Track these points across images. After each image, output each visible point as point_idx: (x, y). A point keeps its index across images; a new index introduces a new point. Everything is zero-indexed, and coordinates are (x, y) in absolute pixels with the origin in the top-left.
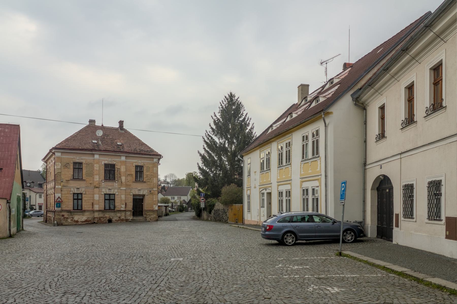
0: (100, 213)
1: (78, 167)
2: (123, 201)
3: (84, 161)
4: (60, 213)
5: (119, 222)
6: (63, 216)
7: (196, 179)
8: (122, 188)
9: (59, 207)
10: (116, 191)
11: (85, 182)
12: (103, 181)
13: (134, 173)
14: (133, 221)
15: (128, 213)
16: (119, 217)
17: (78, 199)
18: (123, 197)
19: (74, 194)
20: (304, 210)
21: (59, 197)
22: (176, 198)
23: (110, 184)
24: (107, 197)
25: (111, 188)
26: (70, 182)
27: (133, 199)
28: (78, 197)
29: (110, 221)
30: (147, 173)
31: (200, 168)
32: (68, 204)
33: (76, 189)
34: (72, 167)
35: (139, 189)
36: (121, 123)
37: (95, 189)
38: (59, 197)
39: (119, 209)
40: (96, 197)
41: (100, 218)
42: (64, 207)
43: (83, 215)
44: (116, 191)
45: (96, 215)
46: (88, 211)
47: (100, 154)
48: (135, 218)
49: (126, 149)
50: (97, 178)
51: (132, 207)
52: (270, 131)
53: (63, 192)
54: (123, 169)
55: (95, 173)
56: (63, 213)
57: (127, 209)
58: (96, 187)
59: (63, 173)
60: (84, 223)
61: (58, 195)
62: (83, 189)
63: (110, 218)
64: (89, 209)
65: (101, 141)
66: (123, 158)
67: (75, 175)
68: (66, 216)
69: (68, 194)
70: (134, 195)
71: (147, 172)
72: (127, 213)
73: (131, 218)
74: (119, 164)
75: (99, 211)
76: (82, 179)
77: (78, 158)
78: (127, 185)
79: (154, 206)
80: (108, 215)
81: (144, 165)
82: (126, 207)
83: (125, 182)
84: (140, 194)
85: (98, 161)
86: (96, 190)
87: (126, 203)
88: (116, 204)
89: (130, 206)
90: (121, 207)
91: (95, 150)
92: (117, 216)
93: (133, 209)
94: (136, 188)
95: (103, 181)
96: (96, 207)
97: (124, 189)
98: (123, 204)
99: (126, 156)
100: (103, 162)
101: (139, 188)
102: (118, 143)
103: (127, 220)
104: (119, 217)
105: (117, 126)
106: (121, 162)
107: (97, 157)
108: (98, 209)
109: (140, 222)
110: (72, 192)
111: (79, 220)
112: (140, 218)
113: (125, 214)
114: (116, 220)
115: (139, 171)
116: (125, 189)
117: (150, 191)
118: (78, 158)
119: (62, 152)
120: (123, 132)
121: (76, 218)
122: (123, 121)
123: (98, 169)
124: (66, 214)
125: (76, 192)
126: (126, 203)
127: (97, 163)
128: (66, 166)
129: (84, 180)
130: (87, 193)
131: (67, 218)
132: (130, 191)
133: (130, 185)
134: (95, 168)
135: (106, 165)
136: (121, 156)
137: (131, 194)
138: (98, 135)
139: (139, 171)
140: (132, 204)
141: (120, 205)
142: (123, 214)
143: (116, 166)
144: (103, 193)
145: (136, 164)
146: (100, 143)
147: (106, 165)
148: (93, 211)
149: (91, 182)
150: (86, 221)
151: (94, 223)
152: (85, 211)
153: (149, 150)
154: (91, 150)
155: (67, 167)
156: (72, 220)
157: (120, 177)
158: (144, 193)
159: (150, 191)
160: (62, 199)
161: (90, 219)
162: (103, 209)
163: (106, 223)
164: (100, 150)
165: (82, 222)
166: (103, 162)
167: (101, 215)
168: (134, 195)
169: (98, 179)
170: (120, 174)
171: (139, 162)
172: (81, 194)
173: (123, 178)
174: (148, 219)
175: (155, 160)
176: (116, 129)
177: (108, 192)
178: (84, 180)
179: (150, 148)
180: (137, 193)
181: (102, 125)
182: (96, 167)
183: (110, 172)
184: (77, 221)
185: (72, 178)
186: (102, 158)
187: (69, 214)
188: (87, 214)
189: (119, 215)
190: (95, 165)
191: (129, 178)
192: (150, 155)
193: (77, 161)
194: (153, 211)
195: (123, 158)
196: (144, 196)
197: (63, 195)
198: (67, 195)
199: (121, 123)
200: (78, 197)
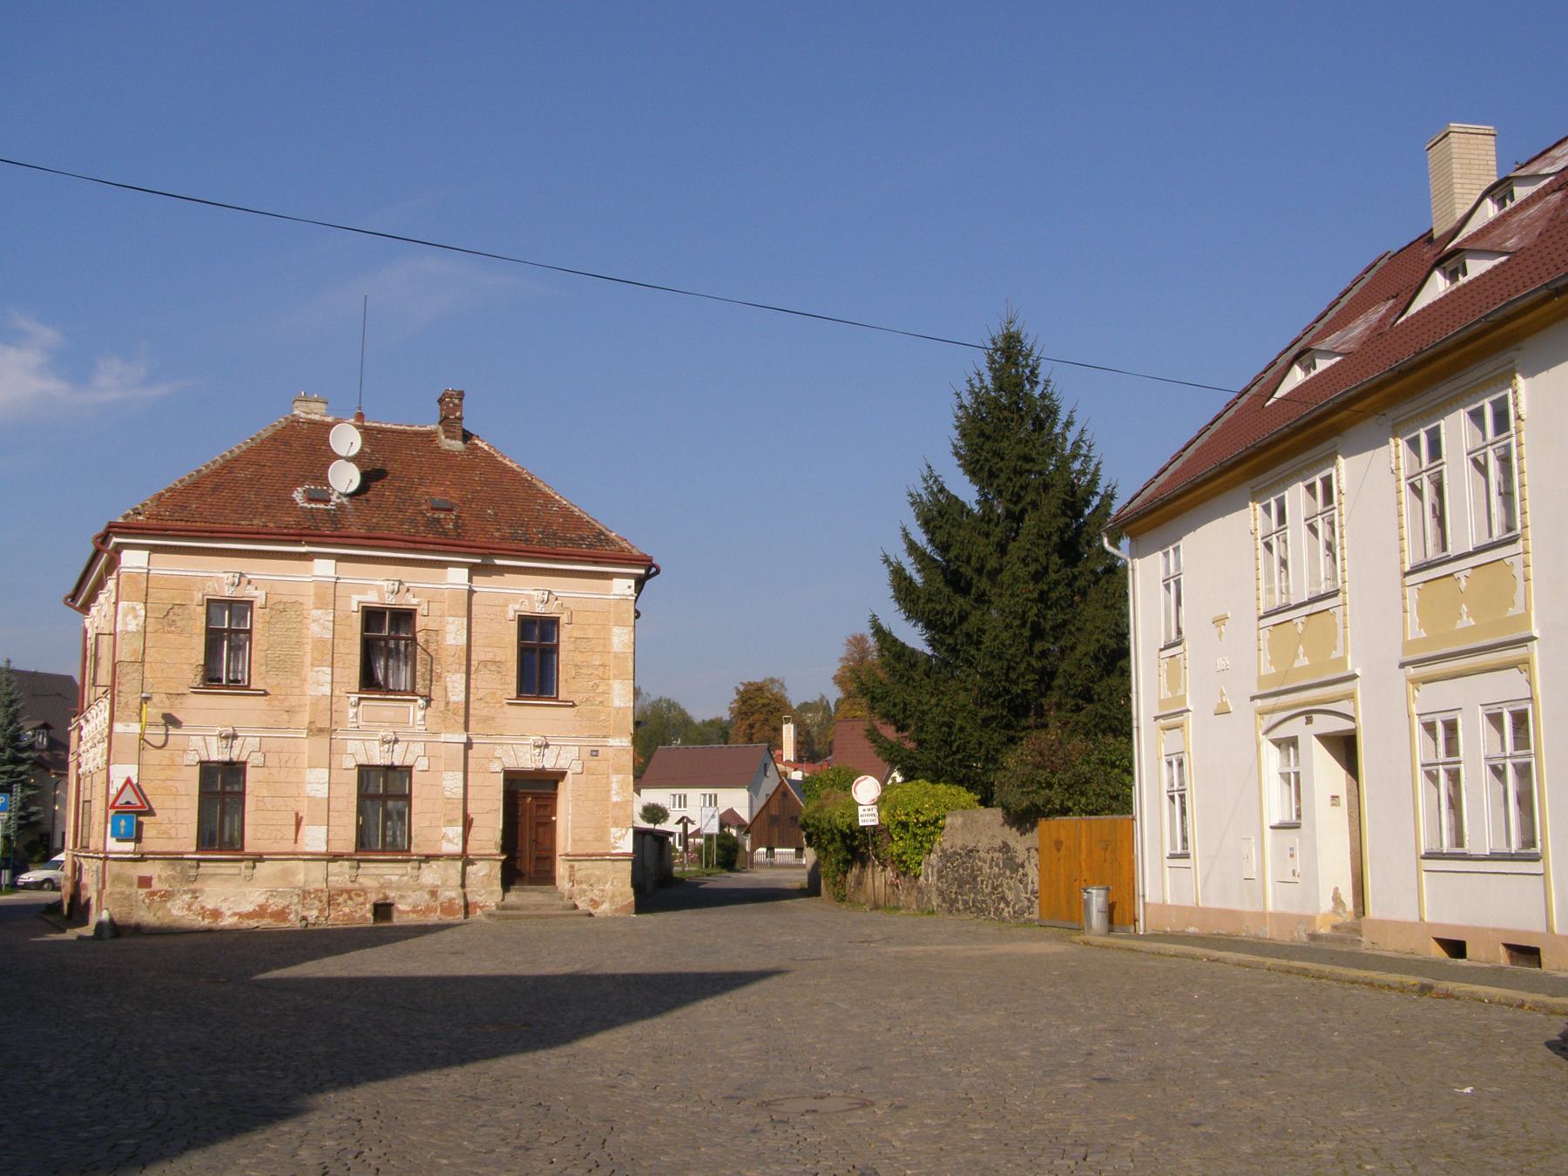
3: (258, 595)
6: (145, 882)
7: (827, 708)
16: (433, 894)
21: (129, 781)
22: (695, 795)
23: (383, 709)
28: (222, 786)
31: (912, 548)
35: (527, 738)
38: (129, 781)
42: (153, 839)
51: (498, 835)
52: (1297, 376)
54: (454, 634)
56: (144, 869)
61: (123, 772)
62: (253, 743)
70: (365, 771)
79: (615, 832)
93: (504, 851)
96: (314, 839)
98: (450, 822)
99: (474, 570)
128: (169, 616)
135: (371, 616)
141: (433, 826)
143: (420, 622)
144: (350, 763)
147: (371, 616)
152: (258, 858)
177: (379, 757)
182: (318, 624)
200: (222, 786)
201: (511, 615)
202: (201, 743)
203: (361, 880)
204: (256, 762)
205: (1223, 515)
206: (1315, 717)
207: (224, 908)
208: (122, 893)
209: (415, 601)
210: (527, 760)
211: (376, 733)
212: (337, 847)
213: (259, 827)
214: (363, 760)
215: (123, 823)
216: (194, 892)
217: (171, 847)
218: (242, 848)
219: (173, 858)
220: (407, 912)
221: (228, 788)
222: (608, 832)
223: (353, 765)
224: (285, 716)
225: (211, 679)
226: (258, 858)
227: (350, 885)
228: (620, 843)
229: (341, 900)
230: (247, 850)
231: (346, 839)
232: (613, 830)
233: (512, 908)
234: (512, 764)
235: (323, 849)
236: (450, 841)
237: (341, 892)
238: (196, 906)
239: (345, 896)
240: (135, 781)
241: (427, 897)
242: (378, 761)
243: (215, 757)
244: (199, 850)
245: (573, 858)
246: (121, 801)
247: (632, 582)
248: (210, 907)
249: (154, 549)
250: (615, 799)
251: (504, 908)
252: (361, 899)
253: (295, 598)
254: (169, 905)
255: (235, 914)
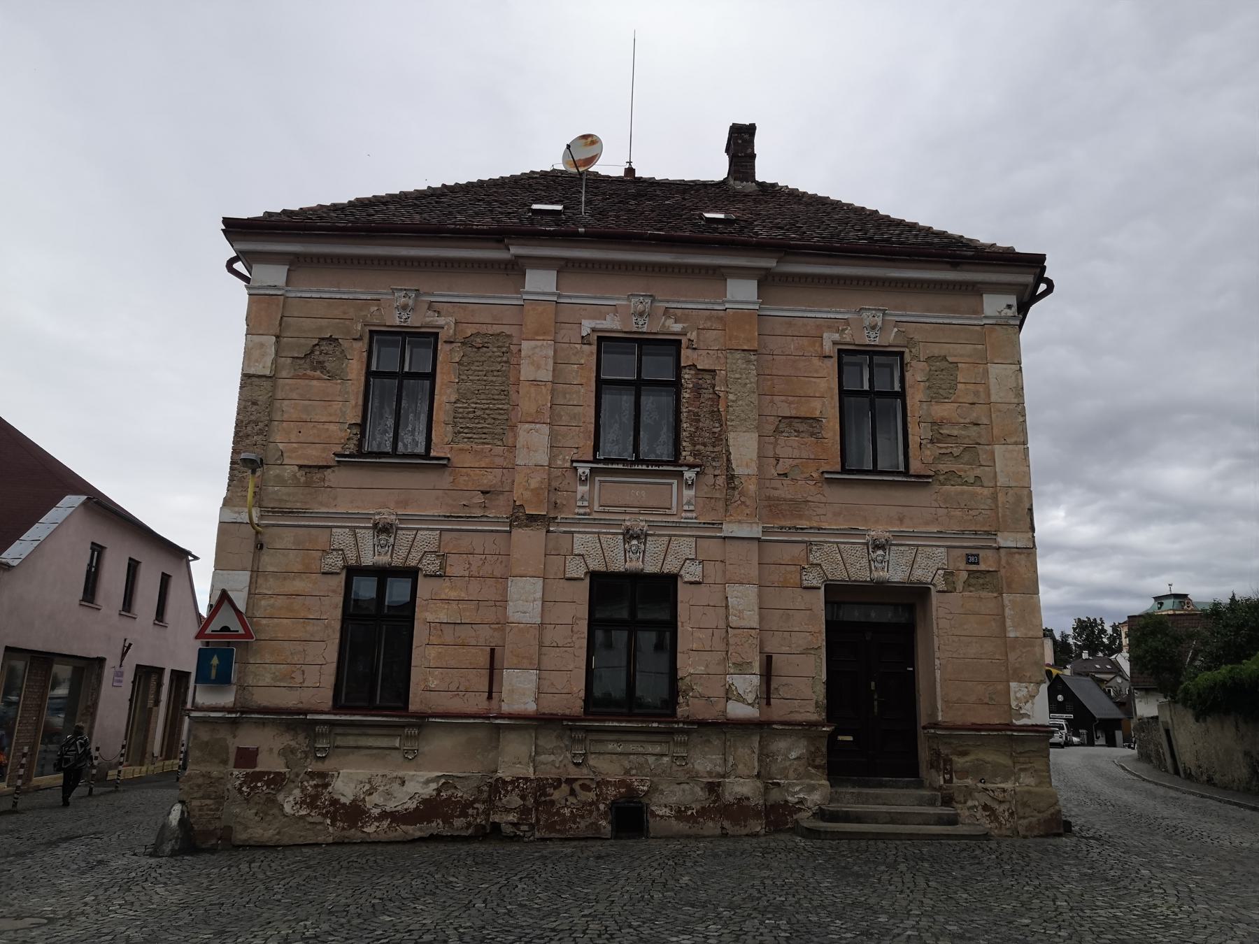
0: (548, 741)
2: (748, 636)
4: (223, 733)
6: (247, 757)
8: (730, 529)
9: (223, 679)
10: (685, 547)
11: (445, 480)
13: (827, 408)
15: (791, 751)
16: (712, 788)
18: (743, 601)
19: (354, 572)
25: (640, 523)
26: (332, 477)
27: (832, 627)
30: (941, 411)
32: (303, 661)
34: (355, 369)
36: (741, 141)
37: (518, 533)
39: (709, 715)
40: (525, 600)
41: (542, 787)
43: (411, 757)
44: (685, 547)
45: (516, 760)
46: (452, 720)
47: (564, 267)
48: (851, 799)
50: (533, 445)
51: (821, 690)
53: (269, 562)
56: (248, 738)
57: (779, 710)
58: (521, 518)
60: (414, 831)
62: (427, 538)
63: (631, 792)
64: (456, 705)
68: (270, 763)
70: (837, 594)
71: (936, 396)
72: (780, 745)
73: (811, 793)
75: (542, 722)
76: (426, 461)
78: (771, 507)
80: (613, 762)
81: (911, 342)
82: (766, 694)
83: (761, 477)
86: (528, 540)
87: (768, 661)
88: (687, 665)
89: (806, 684)
90: (729, 694)
92: (693, 777)
94: (853, 532)
95: (584, 469)
96: (520, 692)
97: (744, 531)
98: (742, 668)
99: (766, 281)
101: (878, 532)
104: (712, 788)
105: (716, 168)
106: (725, 321)
107: (540, 282)
108: (529, 706)
110: (335, 561)
111: (374, 803)
113: (765, 756)
114: (680, 814)
115: (871, 392)
116: (756, 531)
117: (972, 559)
118: (394, 302)
121: (347, 783)
123: (546, 375)
124: (272, 750)
125: (368, 560)
126: (768, 661)
131: (277, 781)
132: (798, 550)
133: (797, 506)
134: (527, 372)
137: (813, 579)
139: (871, 392)
142: (746, 753)
144: (576, 569)
149: (490, 479)
150: (429, 809)
152: (423, 721)
155: (320, 366)
157: (719, 439)
158: (921, 574)
159: (972, 559)
162: (577, 707)
165: (396, 817)
167: (555, 759)
168: (837, 594)
170: (715, 415)
171: (867, 321)
172: (411, 574)
173: (744, 449)
174: (971, 818)
175: (996, 305)
177: (619, 559)
178: (443, 465)
180: (856, 567)
181: (630, 171)
182: (535, 362)
184: (355, 813)
186: (583, 294)
187: (299, 742)
188: (441, 744)
189: (706, 762)
191: (791, 447)
193: (395, 319)
195: (743, 292)
198: (299, 585)
199: (741, 141)
201: (828, 348)
203: (592, 761)
204: (431, 569)
208: (207, 775)
209: (677, 327)
212: (555, 705)
214: (596, 565)
216: (322, 775)
217: (288, 699)
219: (294, 721)
221: (640, 616)
224: (479, 499)
225: (851, 471)
226: (423, 721)
227: (574, 772)
230: (412, 708)
234: (838, 575)
235: (531, 708)
237: (557, 783)
241: (700, 793)
244: (337, 707)
245: (924, 728)
246: (216, 625)
253: (497, 329)
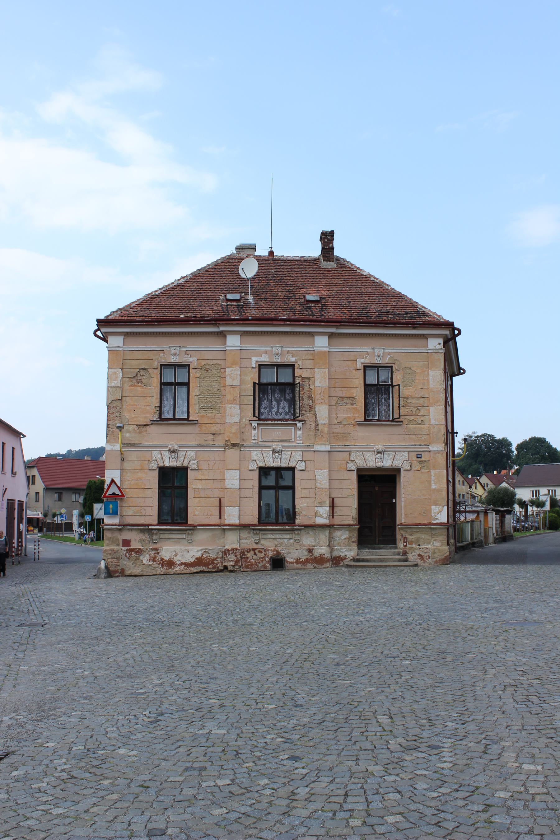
0: (245, 534)
1: (174, 380)
2: (325, 493)
3: (192, 360)
4: (117, 534)
5: (310, 566)
6: (126, 543)
8: (316, 448)
10: (298, 456)
12: (254, 424)
13: (359, 393)
14: (358, 563)
15: (342, 536)
16: (310, 551)
17: (277, 488)
20: (555, 491)
24: (270, 481)
29: (278, 563)
33: (166, 455)
35: (379, 449)
36: (327, 238)
40: (232, 479)
43: (190, 542)
44: (298, 456)
45: (232, 541)
48: (366, 554)
49: (332, 313)
53: (127, 465)
55: (229, 397)
56: (126, 535)
57: (337, 520)
59: (128, 401)
60: (194, 570)
62: (191, 454)
63: (278, 553)
64: (207, 521)
65: (253, 294)
66: (321, 342)
67: (165, 409)
68: (135, 545)
69: (142, 469)
70: (264, 471)
72: (338, 534)
73: (349, 552)
74: (309, 363)
75: (243, 527)
77: (173, 351)
78: (333, 436)
79: (434, 509)
80: (273, 542)
84: (380, 464)
85: (241, 356)
86: (233, 454)
89: (349, 509)
90: (316, 514)
91: (228, 321)
92: (302, 546)
94: (369, 446)
95: (254, 424)
96: (232, 516)
98: (321, 504)
100: (254, 359)
101: (379, 447)
102: (309, 297)
103: (337, 561)
107: (233, 341)
108: (236, 521)
109: (382, 566)
111: (177, 559)
112: (385, 553)
113: (331, 538)
114: (298, 561)
116: (328, 448)
117: (419, 456)
119: (126, 334)
120: (332, 265)
121: (167, 551)
122: (332, 233)
123: (237, 383)
124: (136, 540)
127: (233, 364)
129: (195, 423)
130: (203, 466)
131: (139, 552)
133: (345, 436)
134: (229, 382)
136: (312, 335)
137: (352, 466)
138: (243, 276)
140: (353, 503)
141: (310, 506)
142: (323, 537)
144: (253, 466)
145: (368, 361)
146: (250, 298)
148: (223, 528)
149: (215, 428)
150: (199, 562)
151: (226, 568)
152: (194, 528)
153: (409, 310)
154: (215, 321)
155: (140, 381)
156: (154, 559)
157: (311, 408)
158: (397, 464)
159: (419, 456)
160: (126, 487)
161: (212, 555)
163: (264, 569)
164: (244, 321)
165: (186, 565)
166: (254, 359)
167: (247, 541)
169: (237, 419)
171: (378, 351)
174: (413, 557)
176: (314, 261)
177: (271, 462)
178: (195, 423)
179: (413, 305)
181: (271, 253)
182: (232, 376)
183: (279, 394)
184: (170, 564)
185: (156, 417)
187: (146, 537)
188: (201, 536)
189: (307, 540)
190: (228, 370)
191: (344, 410)
192: (414, 326)
194: (430, 527)
195: (321, 342)
196: (398, 470)
197: (128, 475)
198: (140, 475)
199: (327, 238)
202: (159, 456)
203: (262, 542)
205: (84, 450)
206: (15, 471)
207: (176, 559)
210: (371, 462)
211: (272, 446)
213: (197, 509)
214: (262, 464)
215: (111, 506)
216: (156, 549)
217: (141, 521)
218: (187, 522)
219: (144, 529)
220: (292, 563)
222: (430, 510)
223: (255, 467)
224: (211, 437)
226: (194, 528)
227: (255, 546)
228: (438, 516)
229: (249, 555)
230: (189, 523)
231: (252, 517)
232: (433, 507)
233: (363, 560)
234: (362, 464)
236: (321, 516)
237: (249, 551)
238: (158, 558)
239: (252, 552)
240: (118, 481)
242: (270, 464)
243: (167, 464)
244: (160, 523)
247: (441, 341)
248: (167, 559)
249: (126, 334)
250: (434, 486)
251: (358, 560)
252: (262, 555)
254: (141, 558)
255: (182, 564)
